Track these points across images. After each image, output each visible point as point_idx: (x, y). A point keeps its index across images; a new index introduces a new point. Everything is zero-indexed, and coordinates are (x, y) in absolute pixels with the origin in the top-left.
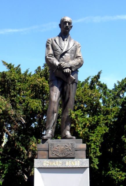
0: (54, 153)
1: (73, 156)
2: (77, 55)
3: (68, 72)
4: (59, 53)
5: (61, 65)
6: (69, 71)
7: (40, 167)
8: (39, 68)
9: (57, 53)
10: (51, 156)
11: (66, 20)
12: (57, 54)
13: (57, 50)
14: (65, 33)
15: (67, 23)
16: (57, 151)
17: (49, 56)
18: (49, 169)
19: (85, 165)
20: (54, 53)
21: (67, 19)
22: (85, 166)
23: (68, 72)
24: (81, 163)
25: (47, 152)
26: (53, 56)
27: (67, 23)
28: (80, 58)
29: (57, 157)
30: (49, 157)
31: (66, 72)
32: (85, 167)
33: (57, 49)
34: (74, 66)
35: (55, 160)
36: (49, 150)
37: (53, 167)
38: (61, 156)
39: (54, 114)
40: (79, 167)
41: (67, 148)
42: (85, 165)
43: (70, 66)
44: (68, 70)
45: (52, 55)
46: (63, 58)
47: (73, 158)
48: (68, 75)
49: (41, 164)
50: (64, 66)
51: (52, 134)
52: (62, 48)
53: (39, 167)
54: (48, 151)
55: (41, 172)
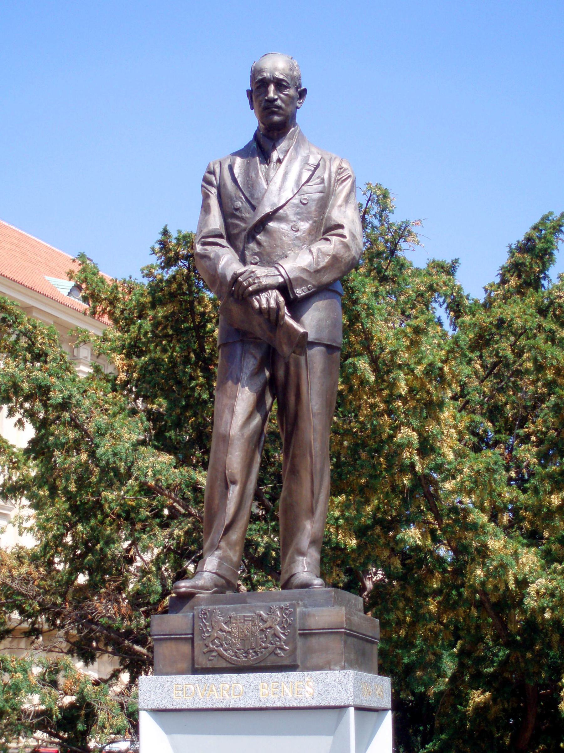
0: (212, 651)
1: (286, 662)
2: (329, 218)
3: (273, 304)
4: (243, 225)
5: (240, 279)
6: (277, 303)
7: (162, 707)
8: (551, 213)
9: (237, 226)
10: (202, 661)
11: (267, 75)
12: (235, 231)
13: (238, 213)
14: (272, 132)
15: (272, 88)
16: (226, 639)
17: (204, 244)
18: (193, 713)
19: (335, 695)
20: (227, 225)
21: (277, 65)
22: (336, 699)
23: (273, 304)
24: (321, 686)
25: (190, 647)
26: (223, 242)
27: (272, 88)
28: (340, 231)
29: (229, 665)
30: (196, 666)
31: (260, 307)
32: (338, 703)
33: (237, 210)
34: (304, 276)
35: (217, 676)
36: (196, 639)
37: (210, 706)
38: (243, 659)
39: (227, 488)
40: (314, 703)
41: (265, 625)
42: (335, 695)
43: (281, 280)
44: (271, 299)
45: (220, 236)
46: (259, 244)
47: (292, 668)
48: (273, 318)
49: (164, 695)
50: (250, 285)
51: (222, 572)
52: (253, 202)
53: (155, 706)
54: (192, 640)
55: (168, 731)
